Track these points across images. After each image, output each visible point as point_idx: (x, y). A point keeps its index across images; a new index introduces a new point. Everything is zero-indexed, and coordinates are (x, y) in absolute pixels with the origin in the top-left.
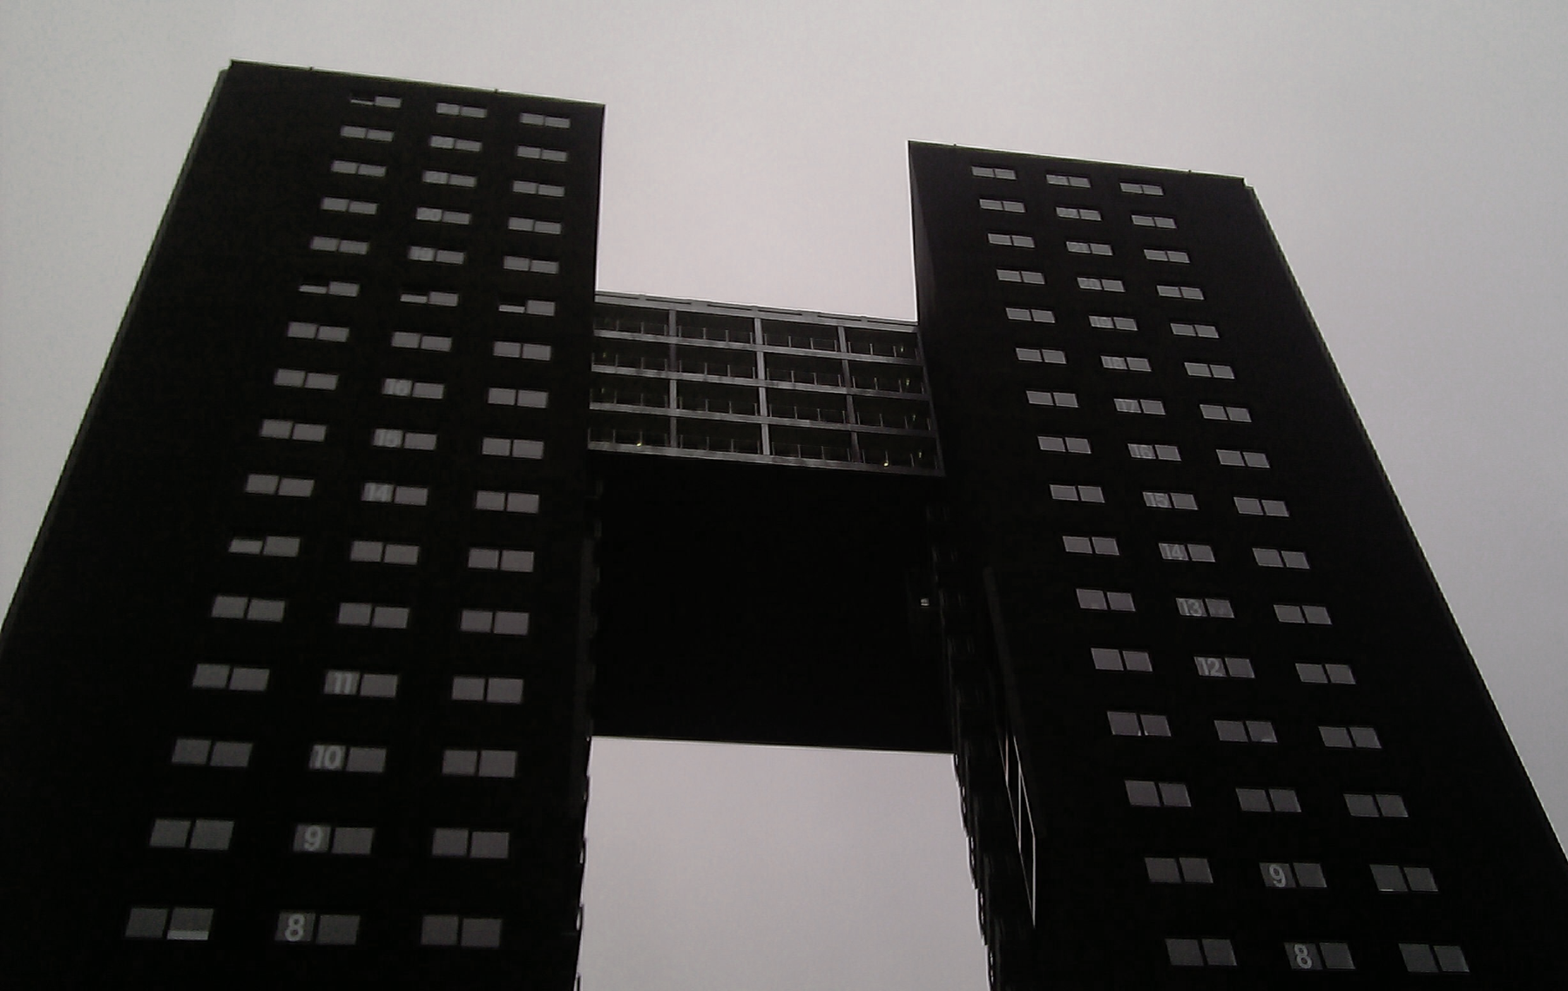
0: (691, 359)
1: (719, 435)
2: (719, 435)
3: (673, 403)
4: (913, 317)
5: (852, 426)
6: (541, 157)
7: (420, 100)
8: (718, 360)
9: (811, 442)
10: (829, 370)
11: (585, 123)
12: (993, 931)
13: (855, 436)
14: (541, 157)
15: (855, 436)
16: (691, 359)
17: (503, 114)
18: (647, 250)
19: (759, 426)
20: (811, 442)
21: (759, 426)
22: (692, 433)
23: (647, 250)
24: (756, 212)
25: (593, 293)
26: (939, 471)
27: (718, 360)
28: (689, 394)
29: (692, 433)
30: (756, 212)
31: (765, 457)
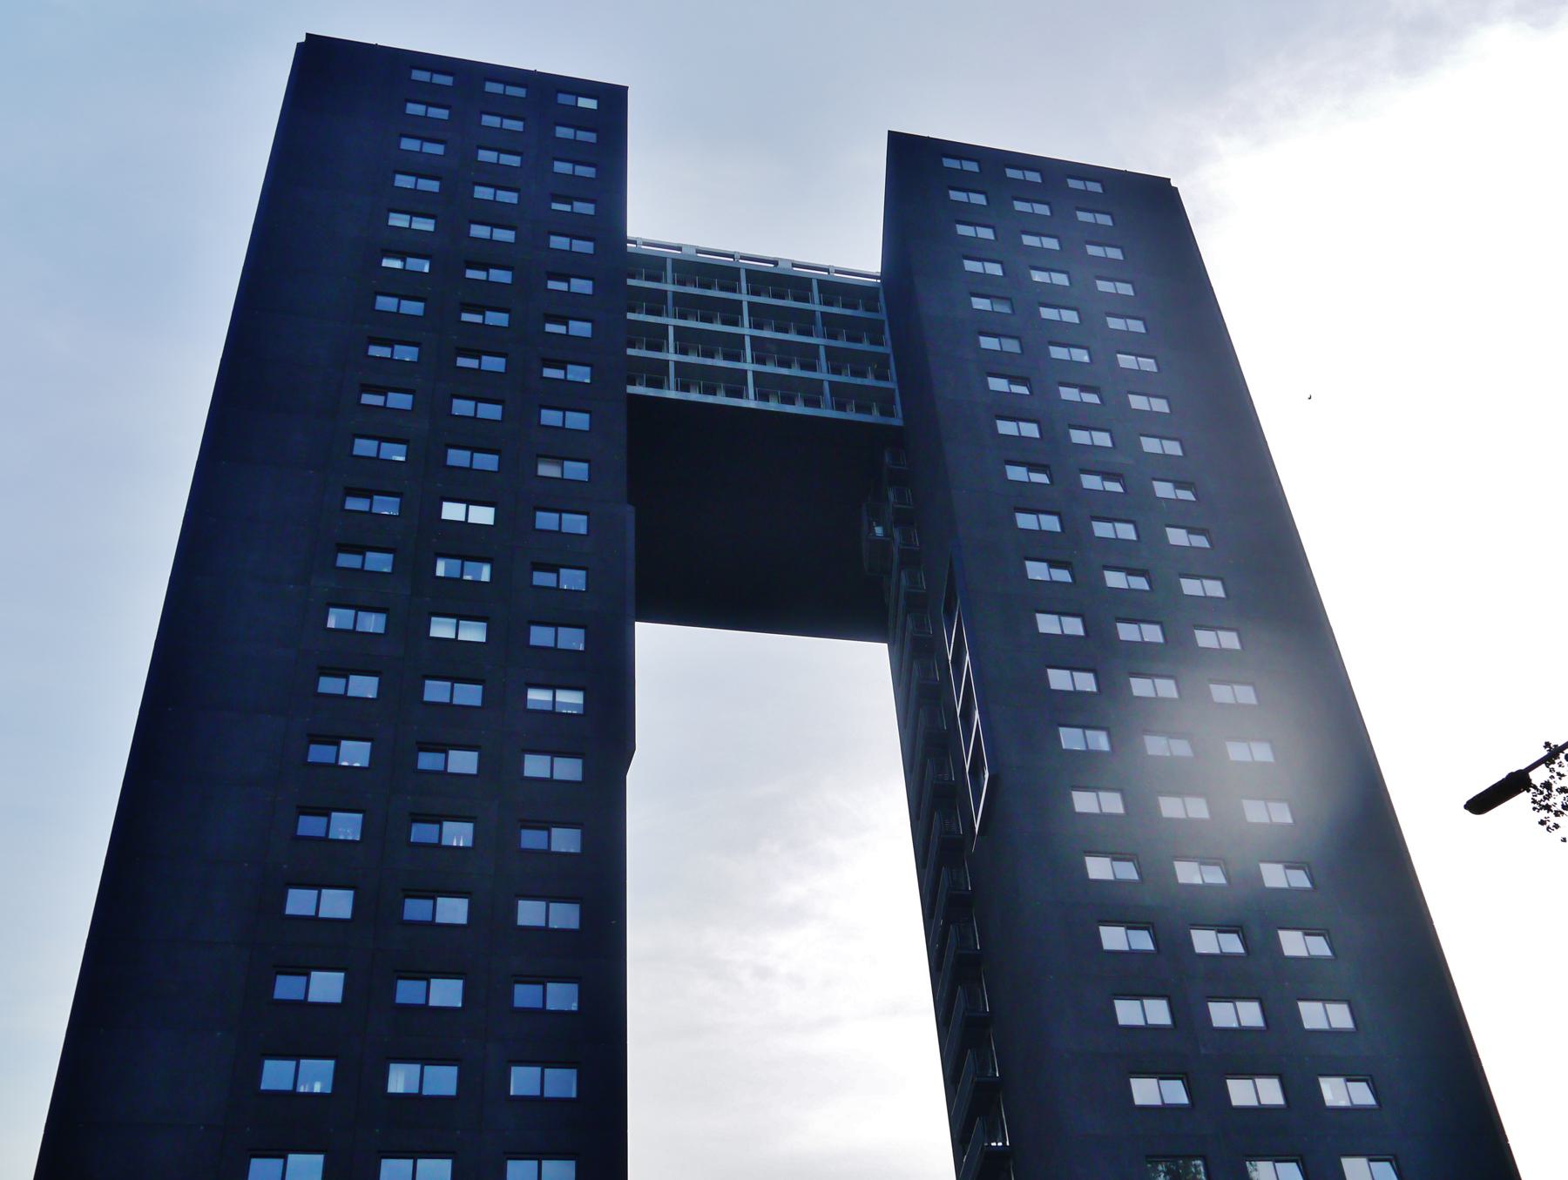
0: (686, 306)
1: (710, 380)
2: (710, 380)
3: (672, 349)
4: (876, 268)
5: (822, 374)
6: (581, 126)
7: (468, 79)
8: (707, 308)
9: (787, 389)
10: (804, 322)
11: (613, 99)
12: (932, 818)
13: (826, 385)
14: (581, 126)
15: (826, 385)
16: (686, 306)
17: (543, 93)
18: (670, 205)
19: (745, 372)
20: (787, 389)
21: (745, 372)
22: (687, 377)
23: (670, 205)
24: (751, 186)
25: (624, 239)
26: (897, 421)
27: (707, 308)
28: (686, 340)
29: (687, 377)
30: (751, 186)
31: (750, 403)
